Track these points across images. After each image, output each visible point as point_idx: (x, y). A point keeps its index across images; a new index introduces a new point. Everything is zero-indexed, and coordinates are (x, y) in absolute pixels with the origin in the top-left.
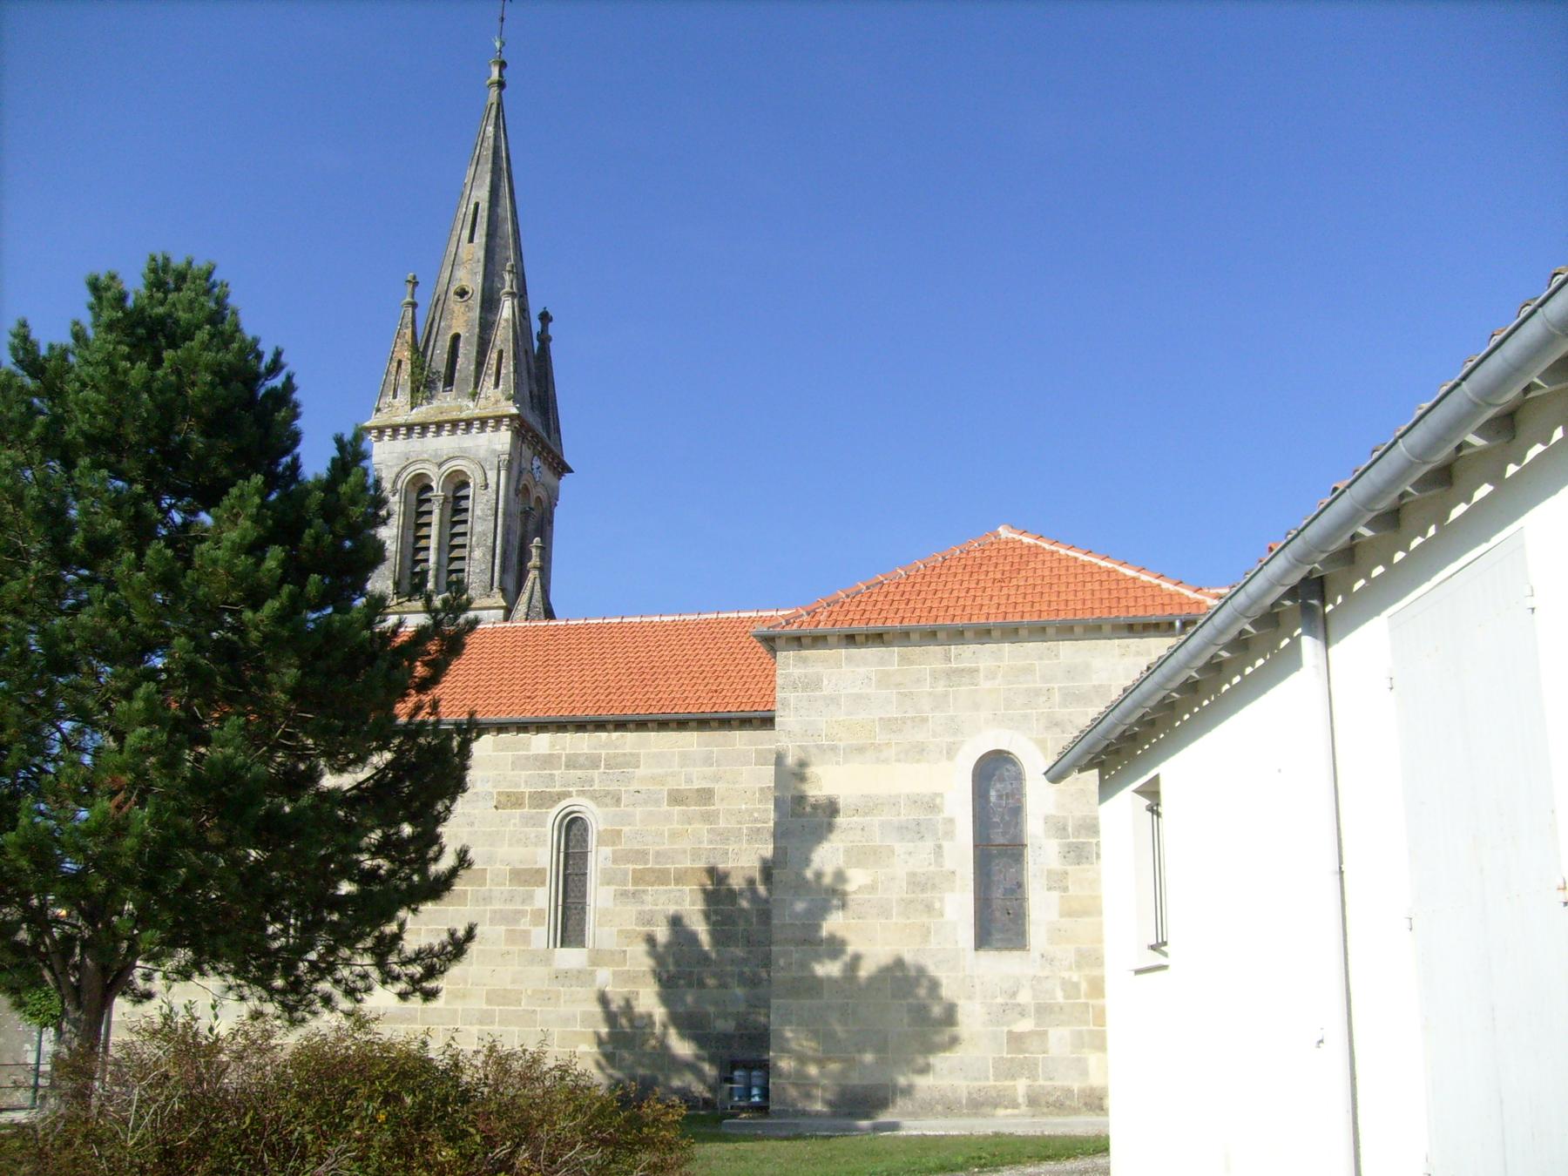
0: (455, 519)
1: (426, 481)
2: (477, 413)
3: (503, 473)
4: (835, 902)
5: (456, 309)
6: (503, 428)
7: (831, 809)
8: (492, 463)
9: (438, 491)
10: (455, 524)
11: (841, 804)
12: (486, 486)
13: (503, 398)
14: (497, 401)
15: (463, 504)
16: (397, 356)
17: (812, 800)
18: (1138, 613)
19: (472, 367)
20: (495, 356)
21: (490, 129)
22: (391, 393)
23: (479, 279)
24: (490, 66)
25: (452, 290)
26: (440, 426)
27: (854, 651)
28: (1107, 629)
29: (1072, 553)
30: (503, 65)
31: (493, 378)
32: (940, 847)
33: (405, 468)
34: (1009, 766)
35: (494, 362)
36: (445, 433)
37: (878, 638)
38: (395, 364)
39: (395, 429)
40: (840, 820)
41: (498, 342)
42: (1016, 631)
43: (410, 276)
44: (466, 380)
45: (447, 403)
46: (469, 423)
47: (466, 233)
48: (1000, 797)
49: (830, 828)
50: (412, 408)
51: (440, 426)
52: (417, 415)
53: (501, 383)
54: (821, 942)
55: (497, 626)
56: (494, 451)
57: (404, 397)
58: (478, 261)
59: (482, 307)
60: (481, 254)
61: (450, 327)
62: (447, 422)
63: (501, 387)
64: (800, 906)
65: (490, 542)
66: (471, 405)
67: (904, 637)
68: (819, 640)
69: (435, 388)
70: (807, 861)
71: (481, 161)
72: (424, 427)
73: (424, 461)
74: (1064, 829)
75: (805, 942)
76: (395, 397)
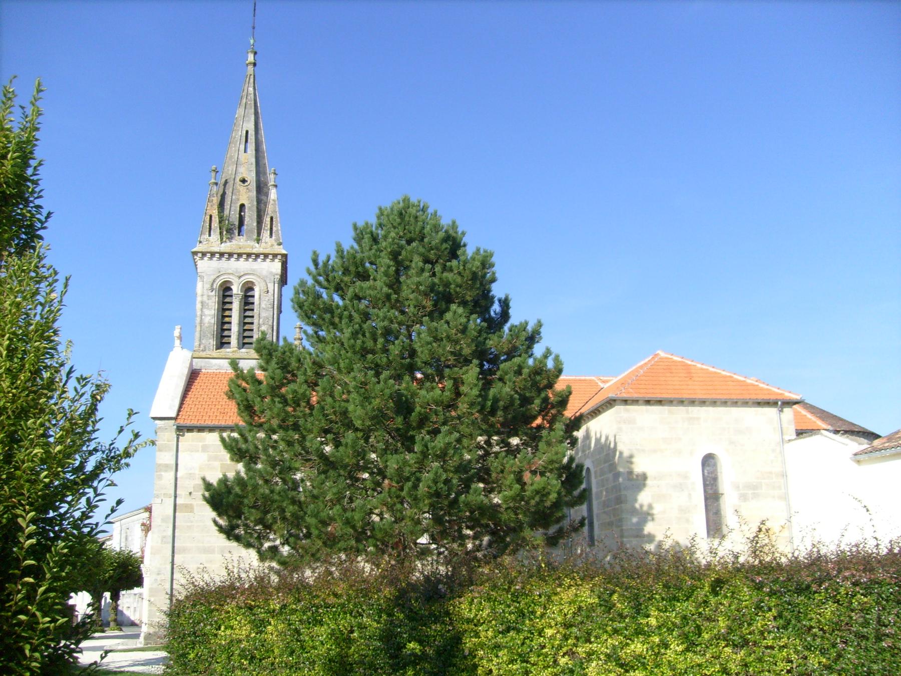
2: (261, 250)
3: (276, 285)
4: (649, 518)
6: (277, 260)
7: (644, 477)
8: (270, 279)
9: (236, 289)
10: (245, 310)
11: (648, 474)
12: (268, 292)
13: (275, 244)
14: (272, 245)
15: (251, 300)
17: (636, 473)
18: (761, 397)
19: (255, 224)
20: (269, 219)
21: (251, 89)
22: (207, 233)
23: (254, 174)
25: (238, 180)
26: (240, 255)
27: (649, 407)
28: (750, 403)
29: (704, 367)
30: (255, 53)
31: (269, 232)
32: (690, 494)
33: (218, 277)
34: (711, 460)
35: (268, 223)
37: (660, 402)
38: (208, 217)
39: (213, 254)
40: (648, 482)
41: (270, 212)
42: (736, 402)
43: (214, 167)
44: (251, 231)
45: (240, 243)
46: (257, 256)
47: (242, 147)
48: (708, 473)
49: (644, 485)
51: (240, 255)
52: (226, 247)
53: (273, 235)
54: (644, 536)
56: (271, 273)
57: (215, 236)
59: (257, 191)
60: (253, 160)
61: (238, 200)
62: (245, 254)
63: (274, 237)
64: (635, 520)
65: (270, 323)
66: (257, 245)
67: (670, 402)
68: (635, 402)
69: (233, 233)
70: (636, 500)
72: (231, 255)
73: (229, 274)
74: (738, 487)
75: (637, 536)
76: (210, 235)
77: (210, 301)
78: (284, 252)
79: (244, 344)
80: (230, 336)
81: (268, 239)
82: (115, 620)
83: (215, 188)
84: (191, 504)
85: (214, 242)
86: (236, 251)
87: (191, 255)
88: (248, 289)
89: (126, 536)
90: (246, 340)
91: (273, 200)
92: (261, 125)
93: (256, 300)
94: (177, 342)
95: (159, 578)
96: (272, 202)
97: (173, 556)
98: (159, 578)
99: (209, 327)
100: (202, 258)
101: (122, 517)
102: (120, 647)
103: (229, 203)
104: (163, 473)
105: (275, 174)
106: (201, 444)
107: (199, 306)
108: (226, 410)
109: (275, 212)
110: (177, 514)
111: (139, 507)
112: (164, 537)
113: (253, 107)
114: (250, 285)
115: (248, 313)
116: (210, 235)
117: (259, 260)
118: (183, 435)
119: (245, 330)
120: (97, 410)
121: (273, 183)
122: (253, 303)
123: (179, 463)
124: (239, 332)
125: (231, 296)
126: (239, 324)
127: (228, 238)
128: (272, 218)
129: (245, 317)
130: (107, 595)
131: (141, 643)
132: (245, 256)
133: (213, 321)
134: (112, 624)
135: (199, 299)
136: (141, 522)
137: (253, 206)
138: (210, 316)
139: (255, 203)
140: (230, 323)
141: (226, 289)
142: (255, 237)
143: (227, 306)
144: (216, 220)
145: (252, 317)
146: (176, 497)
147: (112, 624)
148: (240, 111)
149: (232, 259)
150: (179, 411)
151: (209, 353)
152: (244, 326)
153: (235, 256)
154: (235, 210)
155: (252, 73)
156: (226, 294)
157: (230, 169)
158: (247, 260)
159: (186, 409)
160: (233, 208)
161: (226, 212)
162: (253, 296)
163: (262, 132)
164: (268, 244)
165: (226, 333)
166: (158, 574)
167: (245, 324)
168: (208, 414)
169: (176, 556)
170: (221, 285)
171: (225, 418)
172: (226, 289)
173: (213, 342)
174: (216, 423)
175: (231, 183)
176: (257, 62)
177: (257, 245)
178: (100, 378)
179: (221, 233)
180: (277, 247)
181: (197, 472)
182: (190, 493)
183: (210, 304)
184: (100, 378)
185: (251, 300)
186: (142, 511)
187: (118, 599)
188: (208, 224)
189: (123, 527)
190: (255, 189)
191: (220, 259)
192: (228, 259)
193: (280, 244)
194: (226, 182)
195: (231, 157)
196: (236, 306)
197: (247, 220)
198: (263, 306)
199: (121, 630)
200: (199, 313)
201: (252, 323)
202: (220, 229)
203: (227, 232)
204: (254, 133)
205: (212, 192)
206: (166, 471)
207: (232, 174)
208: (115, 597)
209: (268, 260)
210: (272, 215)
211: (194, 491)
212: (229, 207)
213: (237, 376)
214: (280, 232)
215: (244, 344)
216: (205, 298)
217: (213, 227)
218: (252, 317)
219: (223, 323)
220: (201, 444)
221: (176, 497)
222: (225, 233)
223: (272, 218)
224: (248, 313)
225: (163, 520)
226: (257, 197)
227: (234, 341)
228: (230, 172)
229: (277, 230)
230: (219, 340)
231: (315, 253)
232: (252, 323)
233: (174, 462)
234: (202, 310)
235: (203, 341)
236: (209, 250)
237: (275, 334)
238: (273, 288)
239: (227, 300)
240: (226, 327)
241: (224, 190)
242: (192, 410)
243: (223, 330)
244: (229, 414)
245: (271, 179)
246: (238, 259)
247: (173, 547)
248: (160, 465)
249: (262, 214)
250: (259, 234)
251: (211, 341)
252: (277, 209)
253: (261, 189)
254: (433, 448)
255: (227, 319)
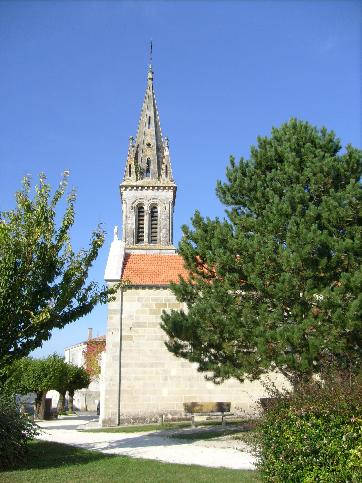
0: (152, 219)
1: (142, 206)
2: (161, 185)
3: (171, 205)
5: (147, 150)
6: (170, 190)
8: (167, 202)
9: (146, 208)
10: (152, 220)
12: (166, 209)
14: (167, 182)
15: (155, 214)
16: (129, 163)
19: (157, 169)
20: (165, 167)
24: (148, 73)
25: (145, 144)
26: (148, 188)
30: (153, 73)
31: (165, 174)
36: (133, 190)
38: (129, 166)
39: (132, 187)
41: (165, 162)
43: (131, 137)
44: (154, 174)
45: (148, 180)
46: (159, 188)
47: (147, 125)
50: (137, 181)
51: (148, 188)
52: (140, 183)
55: (173, 255)
57: (133, 177)
58: (153, 135)
59: (157, 150)
60: (154, 133)
61: (146, 156)
62: (151, 186)
63: (168, 177)
65: (168, 228)
69: (144, 175)
71: (149, 103)
72: (143, 187)
73: (142, 199)
76: (130, 176)
77: (131, 215)
78: (175, 185)
79: (152, 240)
80: (143, 236)
81: (165, 178)
82: (72, 408)
83: (132, 149)
84: (131, 336)
85: (132, 180)
86: (146, 185)
87: (119, 188)
88: (154, 207)
89: (73, 359)
90: (153, 238)
91: (167, 155)
92: (157, 113)
93: (159, 214)
94: (116, 236)
95: (111, 383)
96: (166, 156)
97: (120, 369)
98: (111, 383)
99: (131, 230)
100: (126, 190)
101: (70, 348)
102: (87, 428)
103: (141, 157)
104: (113, 315)
105: (167, 140)
106: (137, 297)
107: (124, 218)
108: (151, 276)
109: (168, 162)
110: (122, 341)
111: (81, 342)
112: (114, 357)
113: (153, 103)
114: (155, 205)
115: (153, 222)
116: (130, 176)
117: (160, 190)
118: (125, 291)
119: (152, 232)
120: (97, 253)
121: (166, 145)
122: (157, 216)
123: (123, 309)
124: (149, 233)
125: (144, 212)
126: (149, 228)
127: (141, 178)
128: (166, 166)
129: (152, 224)
130: (67, 393)
131: (100, 425)
132: (151, 188)
133: (133, 227)
134: (70, 410)
135: (124, 214)
136: (82, 350)
137: (155, 159)
138: (131, 224)
139: (156, 157)
140: (143, 228)
141: (140, 208)
142: (157, 177)
143: (141, 218)
144: (133, 167)
145: (157, 224)
146: (121, 331)
147: (70, 410)
148: (145, 106)
149: (144, 190)
150: (122, 276)
151: (130, 246)
152: (151, 230)
153: (146, 188)
154: (144, 162)
155: (151, 84)
156: (140, 211)
157: (139, 139)
158: (152, 190)
159: (126, 275)
160: (143, 161)
161: (139, 163)
162: (157, 212)
163: (158, 117)
164: (165, 181)
165: (141, 234)
166: (111, 380)
167: (152, 228)
168: (141, 278)
169: (122, 369)
170: (137, 206)
171: (151, 280)
172: (140, 208)
173: (133, 240)
174: (146, 283)
175: (141, 146)
176: (153, 78)
177: (158, 181)
178: (99, 230)
179: (137, 175)
180: (170, 182)
181: (135, 315)
182: (131, 328)
183: (131, 217)
184: (99, 230)
185: (155, 214)
186: (82, 344)
187: (73, 395)
188: (128, 170)
189: (71, 353)
190: (156, 149)
191: (136, 190)
192: (141, 190)
193: (172, 181)
194: (138, 146)
195: (141, 132)
196: (146, 218)
197: (152, 167)
198: (163, 217)
199: (75, 413)
200: (124, 222)
201: (157, 228)
202: (136, 172)
203: (140, 174)
204: (153, 117)
205: (130, 152)
206: (115, 314)
207: (141, 141)
208: (72, 394)
209: (165, 190)
210: (167, 164)
211: (133, 327)
212: (141, 160)
213: (188, 237)
214: (172, 174)
215: (152, 240)
216: (128, 213)
217: (131, 171)
218: (157, 224)
219: (139, 228)
220: (137, 297)
221: (121, 331)
222: (139, 175)
223: (166, 166)
224: (153, 222)
225: (113, 346)
226: (157, 154)
227: (146, 239)
228: (140, 140)
229: (170, 173)
230: (137, 238)
231: (231, 157)
232: (157, 228)
233: (120, 309)
234: (126, 220)
235: (127, 239)
236: (130, 185)
237: (170, 234)
238: (169, 207)
239: (141, 214)
240: (140, 230)
241: (137, 151)
242: (130, 275)
243: (139, 232)
244: (154, 278)
245: (165, 143)
246: (147, 190)
247: (120, 363)
248: (111, 310)
249: (160, 164)
250: (159, 175)
251: (132, 239)
252: (170, 161)
253: (159, 149)
254: (354, 282)
255: (141, 226)
